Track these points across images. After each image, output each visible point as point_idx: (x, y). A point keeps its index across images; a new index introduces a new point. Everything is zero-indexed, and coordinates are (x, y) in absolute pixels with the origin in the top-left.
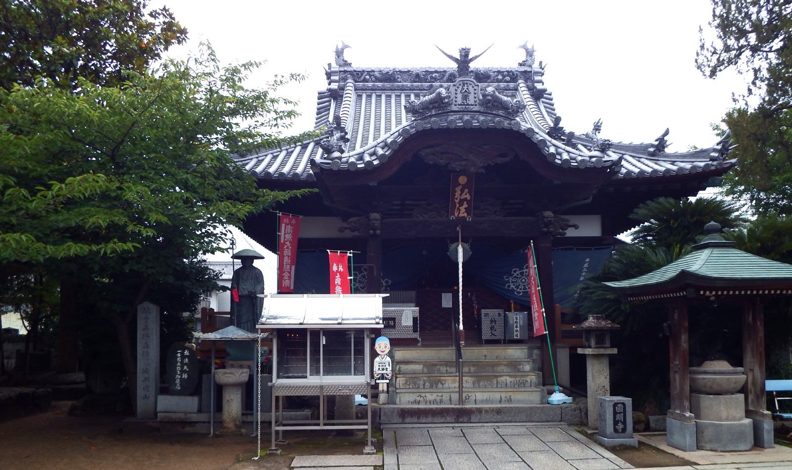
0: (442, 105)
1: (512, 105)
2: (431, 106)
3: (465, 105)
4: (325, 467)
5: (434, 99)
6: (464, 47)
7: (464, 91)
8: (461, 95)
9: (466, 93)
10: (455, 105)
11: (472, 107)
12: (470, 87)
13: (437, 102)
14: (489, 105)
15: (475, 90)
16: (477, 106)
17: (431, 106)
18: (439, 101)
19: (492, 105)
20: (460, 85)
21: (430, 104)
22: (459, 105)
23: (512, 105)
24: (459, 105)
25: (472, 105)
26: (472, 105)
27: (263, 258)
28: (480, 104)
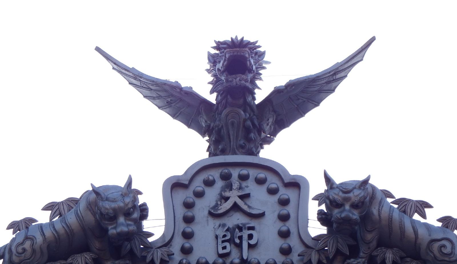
7: (228, 205)
9: (237, 219)
12: (251, 187)
15: (284, 203)
20: (209, 183)
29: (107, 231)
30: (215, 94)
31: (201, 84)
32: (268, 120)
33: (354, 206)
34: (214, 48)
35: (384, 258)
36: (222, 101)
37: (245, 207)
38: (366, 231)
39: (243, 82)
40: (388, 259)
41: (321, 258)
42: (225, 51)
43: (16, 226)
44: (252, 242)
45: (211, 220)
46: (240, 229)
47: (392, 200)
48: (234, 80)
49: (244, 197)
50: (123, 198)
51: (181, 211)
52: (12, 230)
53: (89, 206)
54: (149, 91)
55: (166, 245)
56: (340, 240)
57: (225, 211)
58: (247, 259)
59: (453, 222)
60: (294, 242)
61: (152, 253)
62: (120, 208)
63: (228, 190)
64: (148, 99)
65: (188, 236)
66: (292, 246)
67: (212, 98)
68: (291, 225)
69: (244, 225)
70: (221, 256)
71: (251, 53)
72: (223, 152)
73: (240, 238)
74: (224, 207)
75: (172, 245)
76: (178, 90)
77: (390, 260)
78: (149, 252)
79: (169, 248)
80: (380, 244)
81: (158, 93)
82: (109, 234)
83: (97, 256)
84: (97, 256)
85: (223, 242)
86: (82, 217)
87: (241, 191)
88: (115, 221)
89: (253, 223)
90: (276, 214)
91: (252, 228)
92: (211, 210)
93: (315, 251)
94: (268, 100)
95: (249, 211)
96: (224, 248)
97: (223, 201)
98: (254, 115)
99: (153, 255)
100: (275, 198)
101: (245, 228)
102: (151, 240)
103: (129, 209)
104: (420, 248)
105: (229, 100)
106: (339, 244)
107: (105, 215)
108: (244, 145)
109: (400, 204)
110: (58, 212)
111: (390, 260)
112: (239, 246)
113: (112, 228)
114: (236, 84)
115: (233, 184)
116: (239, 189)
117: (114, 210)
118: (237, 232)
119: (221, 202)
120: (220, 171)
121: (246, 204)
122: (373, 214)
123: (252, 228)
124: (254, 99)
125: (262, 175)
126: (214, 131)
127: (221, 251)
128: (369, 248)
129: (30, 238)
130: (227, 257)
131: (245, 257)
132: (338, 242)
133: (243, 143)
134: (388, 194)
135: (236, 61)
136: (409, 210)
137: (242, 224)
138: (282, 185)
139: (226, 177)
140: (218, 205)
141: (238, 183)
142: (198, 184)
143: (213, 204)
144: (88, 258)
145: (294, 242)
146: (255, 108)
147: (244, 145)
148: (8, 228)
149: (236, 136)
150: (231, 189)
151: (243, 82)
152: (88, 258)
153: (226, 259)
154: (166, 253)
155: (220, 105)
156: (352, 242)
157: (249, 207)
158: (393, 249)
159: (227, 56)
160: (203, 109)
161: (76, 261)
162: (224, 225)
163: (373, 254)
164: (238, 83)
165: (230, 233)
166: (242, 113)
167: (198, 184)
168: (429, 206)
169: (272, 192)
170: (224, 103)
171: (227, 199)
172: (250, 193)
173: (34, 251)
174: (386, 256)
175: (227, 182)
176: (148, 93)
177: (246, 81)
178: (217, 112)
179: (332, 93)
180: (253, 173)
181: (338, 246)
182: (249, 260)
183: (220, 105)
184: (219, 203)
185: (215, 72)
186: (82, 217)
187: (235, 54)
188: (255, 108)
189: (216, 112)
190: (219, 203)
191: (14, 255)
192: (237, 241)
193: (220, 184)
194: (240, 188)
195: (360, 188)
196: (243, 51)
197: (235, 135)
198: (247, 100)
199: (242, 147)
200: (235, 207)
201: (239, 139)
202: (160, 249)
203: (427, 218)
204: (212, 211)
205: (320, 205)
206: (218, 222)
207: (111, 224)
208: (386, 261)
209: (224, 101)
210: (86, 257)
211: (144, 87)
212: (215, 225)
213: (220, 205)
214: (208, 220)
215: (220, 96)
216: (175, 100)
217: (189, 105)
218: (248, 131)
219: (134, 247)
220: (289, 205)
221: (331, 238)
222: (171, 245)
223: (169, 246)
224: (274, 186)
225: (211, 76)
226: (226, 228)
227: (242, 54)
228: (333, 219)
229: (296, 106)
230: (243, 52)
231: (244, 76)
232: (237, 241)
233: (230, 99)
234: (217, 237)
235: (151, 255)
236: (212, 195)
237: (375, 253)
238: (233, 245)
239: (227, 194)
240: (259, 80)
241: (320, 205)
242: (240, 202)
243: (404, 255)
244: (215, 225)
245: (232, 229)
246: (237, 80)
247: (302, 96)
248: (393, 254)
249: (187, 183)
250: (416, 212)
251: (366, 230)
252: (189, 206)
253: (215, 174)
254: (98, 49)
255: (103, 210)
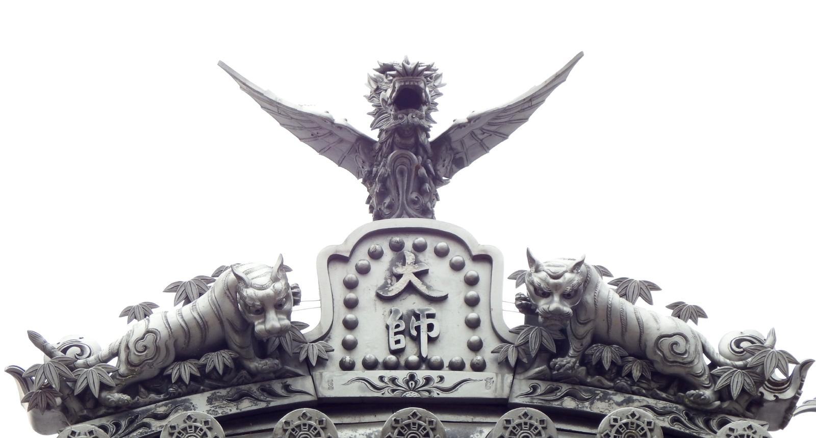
0: (256, 364)
1: (714, 364)
2: (186, 370)
3: (408, 366)
4: (332, 295)
5: (203, 325)
6: (396, 59)
7: (400, 286)
8: (383, 309)
9: (412, 303)
10: (347, 367)
11: (452, 377)
12: (429, 260)
13: (222, 345)
14: (567, 361)
15: (472, 282)
16: (490, 372)
17: (186, 370)
18: (235, 339)
19: (584, 360)
20: (376, 256)
21: (181, 358)
22: (370, 365)
23: (714, 364)
24: (370, 365)
25: (457, 367)
26: (457, 367)
27: (281, 255)
28: (504, 364)
29: (254, 326)
30: (377, 131)
31: (360, 117)
32: (444, 161)
33: (565, 296)
34: (377, 70)
35: (601, 358)
36: (387, 140)
37: (423, 288)
38: (578, 324)
39: (416, 120)
40: (605, 359)
41: (521, 357)
42: (394, 80)
43: (132, 313)
44: (433, 334)
45: (379, 304)
46: (417, 317)
47: (610, 279)
48: (405, 117)
49: (421, 275)
50: (273, 284)
51: (342, 293)
52: (126, 318)
53: (228, 292)
54: (289, 119)
55: (322, 338)
56: (544, 333)
57: (397, 293)
58: (427, 356)
59: (686, 310)
60: (484, 334)
61: (306, 349)
62: (268, 297)
63: (400, 264)
64: (286, 128)
65: (350, 326)
66: (482, 340)
67: (374, 135)
68: (479, 312)
69: (422, 311)
70: (393, 352)
71: (427, 81)
72: (392, 211)
73: (418, 329)
74: (397, 288)
75: (331, 337)
76: (329, 123)
77: (609, 360)
78: (302, 348)
79: (327, 341)
80: (596, 339)
81: (301, 123)
82: (256, 330)
83: (238, 355)
84: (238, 355)
85: (396, 334)
86: (219, 305)
87: (418, 266)
88: (263, 314)
89: (432, 310)
90: (462, 300)
91: (431, 316)
92: (379, 291)
93: (513, 347)
94: (445, 138)
95: (427, 293)
96: (398, 342)
97: (394, 279)
98: (428, 158)
99: (307, 353)
100: (460, 276)
101: (423, 316)
102: (303, 331)
103: (281, 300)
104: (646, 346)
105: (397, 139)
106: (543, 338)
107: (250, 307)
108: (416, 199)
109: (619, 286)
110: (184, 296)
111: (609, 360)
112: (416, 340)
113: (259, 324)
114: (408, 122)
115: (407, 258)
116: (415, 264)
117: (263, 300)
118: (413, 320)
119: (392, 280)
120: (389, 238)
121: (424, 283)
122: (587, 302)
123: (431, 316)
124: (428, 136)
125: (442, 244)
126: (377, 179)
127: (394, 347)
128: (582, 345)
129: (152, 332)
130: (401, 354)
131: (424, 355)
132: (542, 335)
133: (416, 197)
134: (605, 272)
135: (408, 91)
136: (631, 294)
137: (419, 310)
138: (469, 257)
139: (397, 248)
140: (388, 284)
141: (413, 255)
142: (362, 258)
143: (381, 282)
144: (227, 357)
145: (484, 334)
146: (429, 147)
147: (416, 199)
148: (122, 315)
149: (406, 189)
150: (404, 264)
151: (416, 120)
152: (227, 357)
153: (400, 356)
154: (324, 349)
155: (384, 145)
156: (559, 336)
157: (428, 287)
158: (612, 347)
159: (397, 86)
160: (360, 147)
161: (211, 361)
162: (397, 312)
163: (586, 353)
164: (410, 121)
165: (404, 321)
166: (414, 156)
167: (362, 258)
168: (655, 288)
169: (457, 267)
170: (390, 144)
171: (399, 277)
172: (428, 270)
173: (157, 349)
174: (603, 355)
175: (398, 253)
176: (287, 121)
177: (421, 118)
178: (380, 154)
179: (525, 122)
180: (433, 243)
181: (542, 341)
182: (428, 358)
183: (384, 145)
184: (389, 281)
185: (377, 100)
186: (219, 305)
187: (407, 84)
188: (429, 147)
189: (378, 153)
190: (389, 281)
191: (132, 353)
192: (414, 333)
193: (388, 255)
194: (416, 262)
195: (572, 271)
196: (417, 80)
197: (405, 188)
198: (420, 139)
199: (414, 202)
200: (410, 288)
201: (411, 191)
202: (316, 343)
203: (654, 304)
204: (381, 293)
205: (518, 285)
206: (388, 307)
207: (258, 319)
208: (603, 362)
209: (390, 141)
210: (223, 356)
211: (282, 115)
212: (385, 311)
213: (392, 285)
214: (375, 305)
215: (386, 133)
216: (320, 132)
217: (341, 141)
218: (421, 181)
219: (283, 341)
220: (476, 286)
221: (533, 330)
222: (329, 337)
223: (327, 338)
224: (460, 259)
225: (373, 106)
226: (399, 316)
227: (416, 84)
228: (537, 310)
229: (480, 141)
230: (418, 82)
231: (418, 112)
232: (414, 333)
233: (398, 139)
234: (387, 327)
235: (305, 353)
236: (379, 270)
237: (589, 352)
238: (408, 338)
239: (399, 270)
240: (435, 111)
241: (518, 285)
242: (416, 282)
243: (625, 353)
244: (385, 311)
245: (406, 316)
246: (410, 117)
247: (488, 130)
248: (612, 352)
249: (347, 255)
250: (640, 296)
251: (578, 322)
252: (351, 285)
253: (382, 244)
254: (222, 65)
255: (248, 301)
